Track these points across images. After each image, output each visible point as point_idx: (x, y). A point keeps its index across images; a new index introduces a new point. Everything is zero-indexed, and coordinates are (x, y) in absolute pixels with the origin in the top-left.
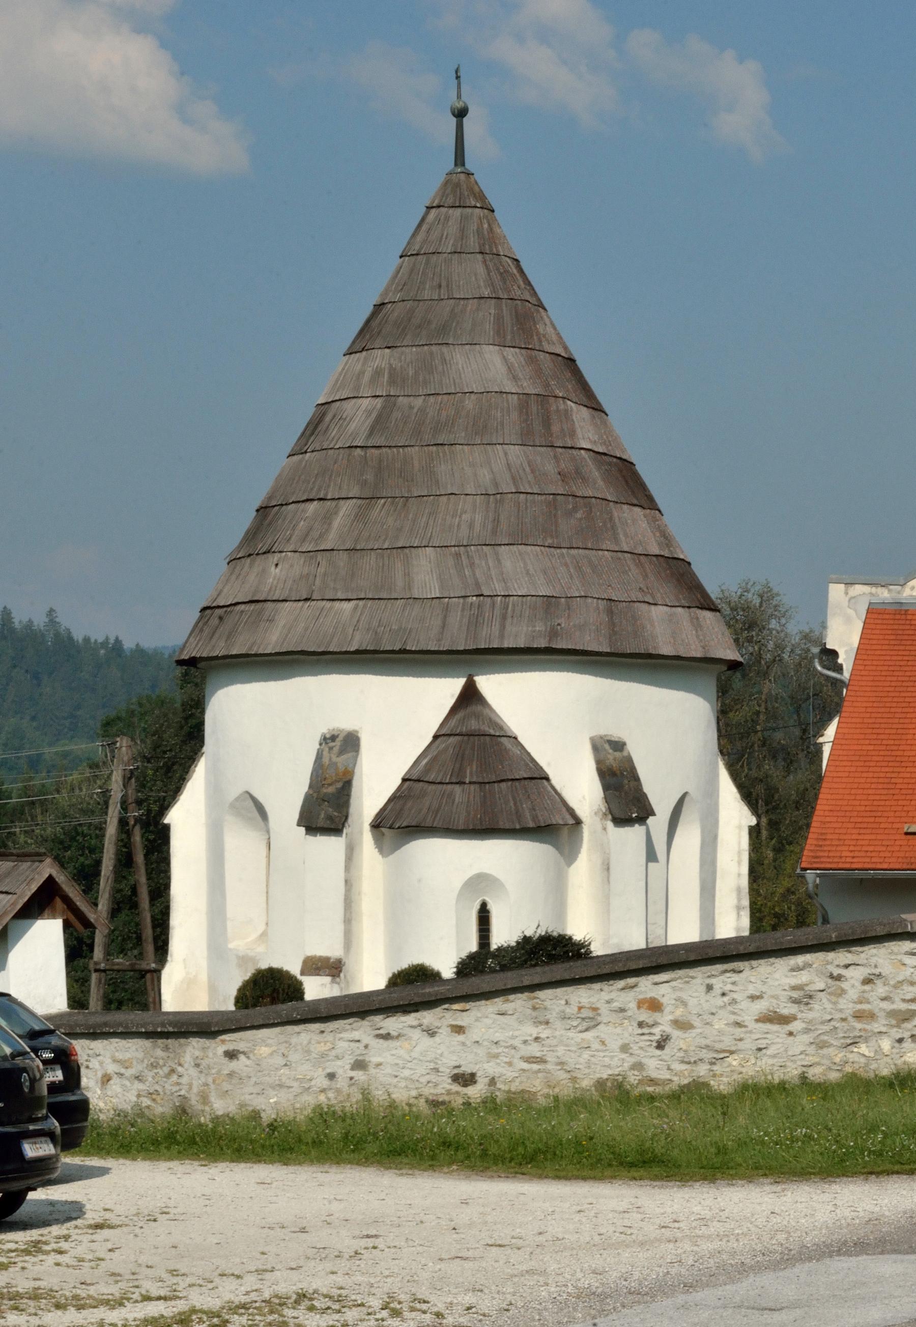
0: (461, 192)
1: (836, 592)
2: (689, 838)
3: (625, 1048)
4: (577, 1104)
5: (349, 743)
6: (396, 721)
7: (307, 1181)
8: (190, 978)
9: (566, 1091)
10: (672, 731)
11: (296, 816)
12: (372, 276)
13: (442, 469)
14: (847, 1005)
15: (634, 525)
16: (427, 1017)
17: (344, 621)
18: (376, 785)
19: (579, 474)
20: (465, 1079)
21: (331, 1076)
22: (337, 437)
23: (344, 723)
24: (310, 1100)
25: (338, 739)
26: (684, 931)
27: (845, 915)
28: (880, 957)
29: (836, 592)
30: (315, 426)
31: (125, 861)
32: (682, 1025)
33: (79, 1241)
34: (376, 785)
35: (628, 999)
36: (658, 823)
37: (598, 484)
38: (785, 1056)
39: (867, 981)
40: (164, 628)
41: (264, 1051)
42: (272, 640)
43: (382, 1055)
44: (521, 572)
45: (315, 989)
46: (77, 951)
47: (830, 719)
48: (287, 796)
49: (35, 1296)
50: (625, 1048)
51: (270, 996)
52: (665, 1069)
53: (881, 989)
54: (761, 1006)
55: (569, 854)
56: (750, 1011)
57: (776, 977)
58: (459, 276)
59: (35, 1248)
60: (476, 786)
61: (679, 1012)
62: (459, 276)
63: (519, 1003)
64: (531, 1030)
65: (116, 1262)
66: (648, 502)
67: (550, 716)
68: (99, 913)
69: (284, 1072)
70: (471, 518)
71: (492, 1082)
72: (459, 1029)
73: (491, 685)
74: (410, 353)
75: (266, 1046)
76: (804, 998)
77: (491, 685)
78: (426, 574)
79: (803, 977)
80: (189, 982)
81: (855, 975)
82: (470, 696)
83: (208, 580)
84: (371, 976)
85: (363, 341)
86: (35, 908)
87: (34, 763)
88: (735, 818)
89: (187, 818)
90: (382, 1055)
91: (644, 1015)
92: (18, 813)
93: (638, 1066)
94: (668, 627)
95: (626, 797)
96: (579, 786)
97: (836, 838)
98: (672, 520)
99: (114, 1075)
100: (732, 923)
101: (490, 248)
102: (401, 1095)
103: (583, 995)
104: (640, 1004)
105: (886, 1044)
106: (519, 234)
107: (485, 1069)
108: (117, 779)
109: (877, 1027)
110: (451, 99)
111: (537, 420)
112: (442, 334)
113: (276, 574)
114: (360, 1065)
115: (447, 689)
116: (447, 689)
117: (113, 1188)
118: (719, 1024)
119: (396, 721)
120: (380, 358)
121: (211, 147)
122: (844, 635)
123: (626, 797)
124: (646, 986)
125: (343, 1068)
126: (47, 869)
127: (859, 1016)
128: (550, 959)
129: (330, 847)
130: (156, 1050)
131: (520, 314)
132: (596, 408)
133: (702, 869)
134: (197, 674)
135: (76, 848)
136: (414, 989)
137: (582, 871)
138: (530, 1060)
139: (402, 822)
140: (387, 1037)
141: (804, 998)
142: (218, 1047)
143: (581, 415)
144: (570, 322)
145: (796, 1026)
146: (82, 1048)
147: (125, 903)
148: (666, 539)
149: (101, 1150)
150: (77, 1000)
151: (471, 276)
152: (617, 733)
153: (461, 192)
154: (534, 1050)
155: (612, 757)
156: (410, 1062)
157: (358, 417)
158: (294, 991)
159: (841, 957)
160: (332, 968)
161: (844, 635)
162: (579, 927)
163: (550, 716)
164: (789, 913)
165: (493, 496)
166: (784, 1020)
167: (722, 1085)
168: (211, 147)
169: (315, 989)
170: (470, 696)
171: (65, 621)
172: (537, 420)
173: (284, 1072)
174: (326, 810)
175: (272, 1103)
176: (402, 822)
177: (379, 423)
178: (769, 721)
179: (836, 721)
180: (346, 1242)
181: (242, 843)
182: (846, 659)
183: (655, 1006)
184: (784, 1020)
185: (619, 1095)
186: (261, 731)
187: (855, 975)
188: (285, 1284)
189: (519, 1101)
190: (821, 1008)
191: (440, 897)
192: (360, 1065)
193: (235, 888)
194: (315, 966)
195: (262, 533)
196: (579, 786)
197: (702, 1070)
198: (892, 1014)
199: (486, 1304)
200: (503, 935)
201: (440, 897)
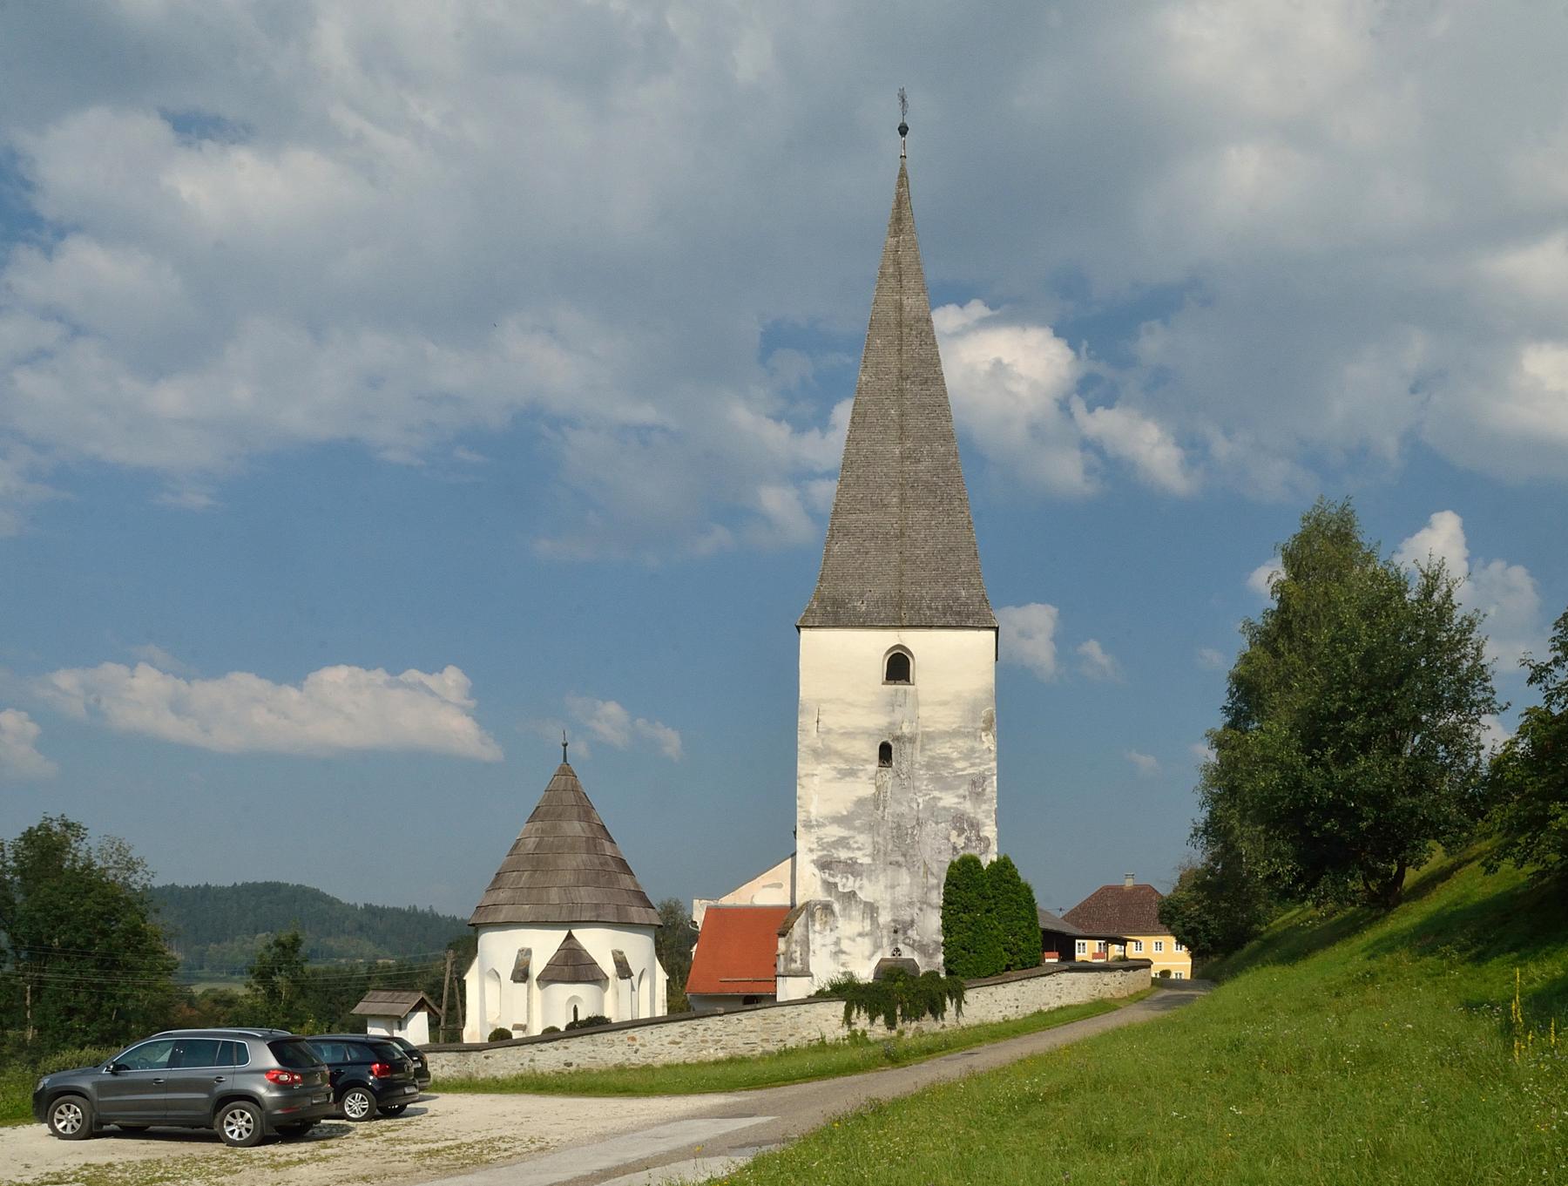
0: (566, 770)
1: (696, 902)
2: (646, 983)
4: (608, 1072)
5: (529, 952)
6: (544, 945)
8: (473, 1031)
9: (603, 1068)
10: (639, 948)
11: (1025, 875)
12: (536, 797)
13: (560, 862)
14: (698, 1038)
15: (625, 880)
16: (555, 1044)
17: (526, 911)
18: (537, 967)
19: (606, 863)
20: (570, 1065)
22: (523, 850)
23: (527, 946)
24: (514, 1073)
25: (831, 880)
26: (645, 1014)
27: (700, 1008)
28: (709, 1022)
29: (696, 902)
30: (516, 846)
31: (452, 990)
33: (424, 1121)
34: (537, 967)
35: (625, 1037)
36: (635, 978)
37: (613, 867)
38: (678, 1055)
40: (466, 913)
42: (501, 918)
43: (539, 1057)
44: (585, 895)
45: (516, 1035)
46: (433, 1025)
48: (507, 970)
49: (407, 1140)
51: (501, 1037)
52: (637, 1060)
55: (605, 988)
57: (674, 1029)
58: (565, 800)
59: (409, 1123)
60: (573, 966)
62: (565, 800)
63: (587, 1038)
65: (438, 1128)
66: (631, 873)
67: (598, 943)
68: (442, 1012)
69: (505, 1063)
70: (569, 878)
73: (578, 933)
74: (548, 823)
75: (498, 1054)
76: (684, 1036)
77: (578, 933)
78: (554, 895)
80: (473, 1033)
81: (701, 1028)
82: (570, 936)
83: (479, 897)
84: (536, 1030)
85: (532, 819)
86: (416, 1009)
87: (425, 958)
88: (661, 977)
89: (472, 979)
90: (539, 1057)
92: (418, 975)
94: (636, 913)
95: (624, 970)
96: (608, 967)
97: (698, 982)
98: (638, 879)
99: (441, 1065)
100: (661, 1011)
101: (575, 789)
102: (546, 1071)
103: (608, 1036)
106: (584, 784)
107: (576, 1061)
108: (448, 966)
111: (592, 845)
112: (560, 816)
113: (502, 895)
115: (563, 934)
116: (563, 934)
117: (441, 1103)
119: (544, 945)
120: (538, 824)
121: (491, 752)
122: (699, 916)
123: (624, 970)
124: (630, 1032)
125: (526, 1062)
126: (421, 995)
128: (597, 1025)
129: (523, 986)
130: (460, 1056)
131: (586, 811)
132: (612, 842)
133: (649, 993)
134: (477, 928)
135: (435, 990)
136: (551, 1035)
137: (609, 995)
139: (547, 978)
141: (684, 1036)
142: (482, 1055)
143: (607, 844)
144: (603, 814)
146: (428, 1057)
147: (451, 1008)
148: (637, 885)
149: (437, 1090)
150: (434, 1036)
151: (570, 798)
153: (566, 770)
156: (549, 1059)
157: (531, 843)
158: (509, 1035)
159: (696, 1022)
160: (523, 1028)
161: (699, 916)
162: (609, 1013)
163: (598, 943)
164: (681, 1007)
165: (577, 870)
167: (658, 1065)
168: (491, 752)
169: (516, 1035)
170: (570, 936)
171: (436, 910)
172: (592, 845)
173: (505, 1063)
174: (521, 974)
175: (501, 1074)
176: (547, 978)
177: (538, 846)
178: (673, 943)
180: (519, 1119)
181: (491, 987)
182: (699, 924)
183: (634, 1039)
185: (620, 1069)
186: (498, 948)
187: (701, 1028)
188: (496, 1134)
189: (588, 1072)
190: (689, 1039)
191: (559, 1004)
193: (490, 1000)
194: (516, 1027)
195: (496, 885)
196: (608, 967)
197: (650, 1061)
199: (564, 1138)
200: (581, 1017)
201: (559, 1004)
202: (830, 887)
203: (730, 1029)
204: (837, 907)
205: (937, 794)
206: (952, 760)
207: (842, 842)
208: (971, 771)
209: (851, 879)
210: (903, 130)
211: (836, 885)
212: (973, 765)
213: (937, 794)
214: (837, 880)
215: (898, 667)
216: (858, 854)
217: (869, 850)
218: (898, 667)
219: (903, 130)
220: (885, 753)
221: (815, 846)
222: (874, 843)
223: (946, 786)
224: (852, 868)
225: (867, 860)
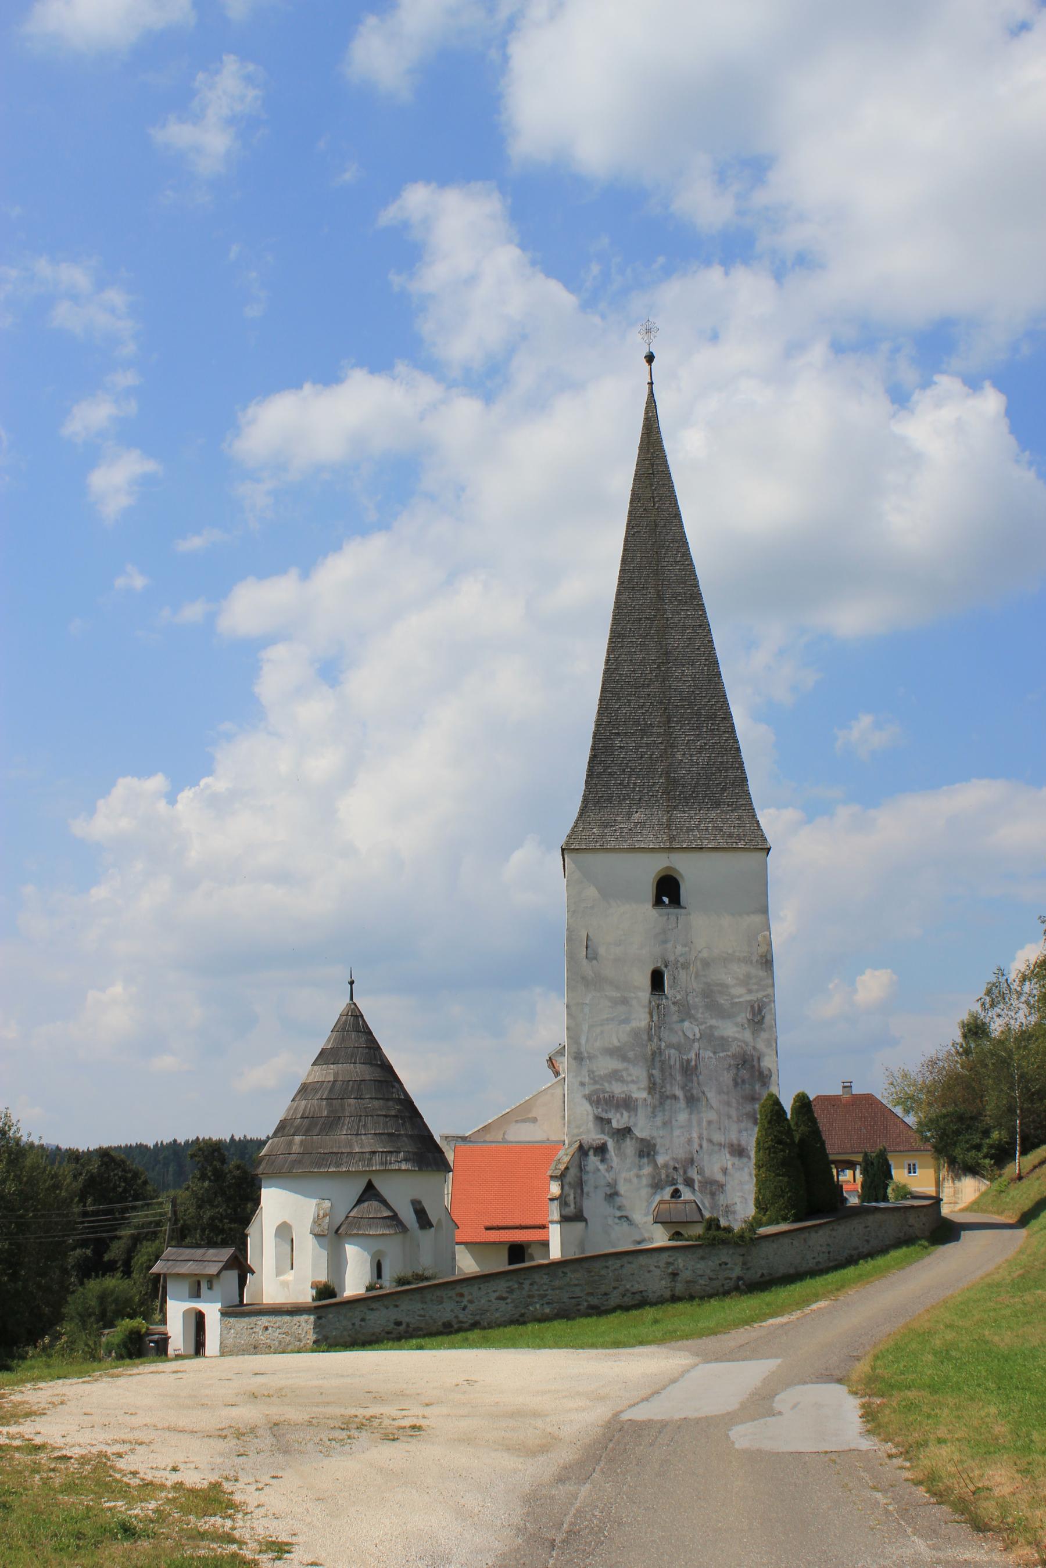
3: (452, 1311)
7: (120, 1455)
14: (525, 1293)
21: (353, 1324)
25: (605, 1116)
32: (471, 1302)
35: (452, 1293)
39: (531, 1284)
41: (331, 1316)
43: (371, 1316)
47: (776, 1357)
50: (452, 1311)
53: (536, 1287)
54: (497, 1294)
56: (494, 1296)
61: (470, 1297)
64: (420, 1306)
71: (408, 1325)
72: (397, 1306)
79: (510, 1284)
91: (458, 1299)
93: (457, 1317)
104: (457, 1295)
105: (538, 1306)
107: (405, 1319)
109: (535, 1300)
110: (349, 979)
114: (363, 1320)
118: (483, 1301)
127: (529, 1296)
138: (420, 1316)
140: (372, 1309)
141: (511, 1291)
145: (509, 1301)
152: (417, 1197)
154: (422, 1312)
155: (418, 1207)
166: (504, 1299)
179: (779, 1361)
183: (462, 1295)
184: (504, 1299)
187: (527, 1283)
192: (363, 1320)
196: (408, 1216)
198: (539, 1295)
202: (602, 1122)
203: (557, 1283)
204: (611, 1145)
205: (713, 1022)
206: (727, 986)
207: (615, 1076)
208: (748, 998)
209: (626, 1114)
210: (650, 358)
211: (609, 1121)
212: (750, 991)
213: (713, 1022)
214: (610, 1115)
215: (667, 890)
216: (633, 1087)
217: (644, 1083)
218: (667, 890)
219: (650, 358)
220: (657, 980)
221: (587, 1080)
222: (651, 1076)
223: (722, 1013)
224: (627, 1104)
225: (644, 1095)
